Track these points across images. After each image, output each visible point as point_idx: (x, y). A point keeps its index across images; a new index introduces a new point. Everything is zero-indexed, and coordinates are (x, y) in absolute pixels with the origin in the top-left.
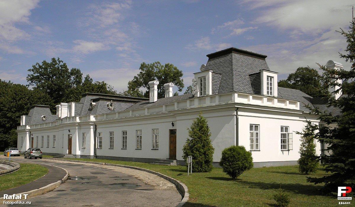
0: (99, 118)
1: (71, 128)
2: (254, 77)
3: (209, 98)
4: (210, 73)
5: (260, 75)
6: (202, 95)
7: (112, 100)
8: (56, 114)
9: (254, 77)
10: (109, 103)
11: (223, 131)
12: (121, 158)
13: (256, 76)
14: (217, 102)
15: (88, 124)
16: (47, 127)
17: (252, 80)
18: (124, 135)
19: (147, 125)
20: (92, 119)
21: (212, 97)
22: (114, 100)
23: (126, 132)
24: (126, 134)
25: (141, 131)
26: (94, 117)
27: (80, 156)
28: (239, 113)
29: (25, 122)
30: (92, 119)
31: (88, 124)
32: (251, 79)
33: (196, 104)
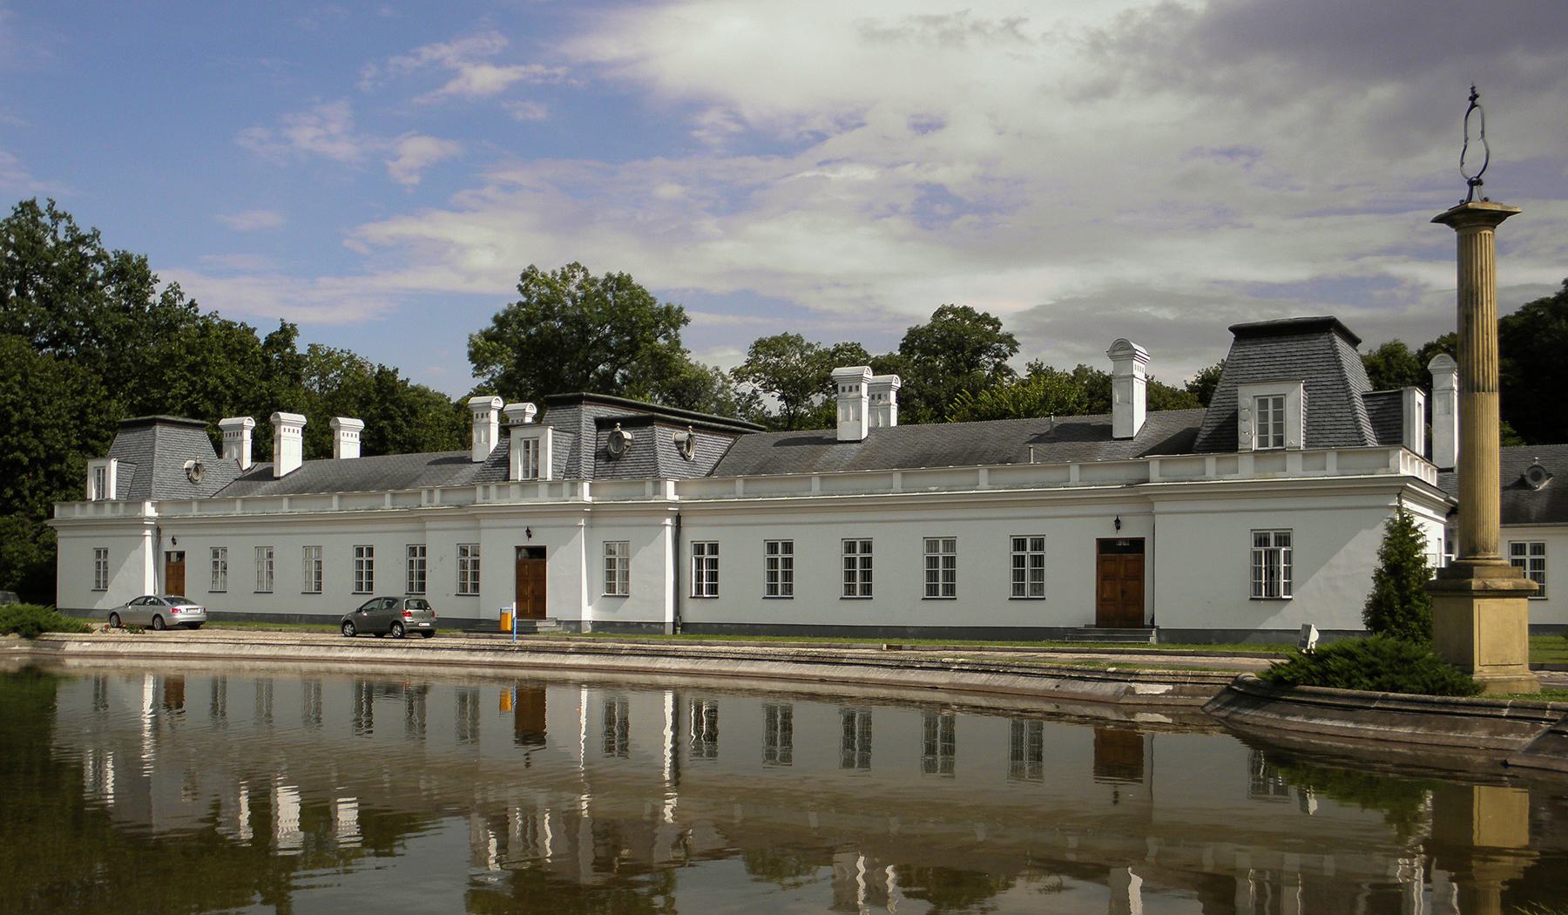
0: (692, 490)
1: (539, 522)
2: (1381, 403)
3: (546, 486)
4: (550, 431)
5: (1401, 399)
6: (528, 477)
7: (690, 424)
8: (331, 456)
9: (1381, 403)
10: (682, 435)
11: (1350, 546)
12: (700, 626)
13: (1387, 402)
14: (121, 511)
15: (139, 523)
16: (296, 511)
17: (1372, 410)
18: (100, 557)
19: (358, 535)
20: (149, 510)
21: (115, 504)
22: (697, 427)
23: (106, 552)
24: (105, 557)
25: (319, 548)
26: (153, 505)
27: (590, 627)
28: (1158, 507)
29: (117, 478)
30: (149, 510)
31: (139, 523)
32: (1370, 408)
33: (514, 498)
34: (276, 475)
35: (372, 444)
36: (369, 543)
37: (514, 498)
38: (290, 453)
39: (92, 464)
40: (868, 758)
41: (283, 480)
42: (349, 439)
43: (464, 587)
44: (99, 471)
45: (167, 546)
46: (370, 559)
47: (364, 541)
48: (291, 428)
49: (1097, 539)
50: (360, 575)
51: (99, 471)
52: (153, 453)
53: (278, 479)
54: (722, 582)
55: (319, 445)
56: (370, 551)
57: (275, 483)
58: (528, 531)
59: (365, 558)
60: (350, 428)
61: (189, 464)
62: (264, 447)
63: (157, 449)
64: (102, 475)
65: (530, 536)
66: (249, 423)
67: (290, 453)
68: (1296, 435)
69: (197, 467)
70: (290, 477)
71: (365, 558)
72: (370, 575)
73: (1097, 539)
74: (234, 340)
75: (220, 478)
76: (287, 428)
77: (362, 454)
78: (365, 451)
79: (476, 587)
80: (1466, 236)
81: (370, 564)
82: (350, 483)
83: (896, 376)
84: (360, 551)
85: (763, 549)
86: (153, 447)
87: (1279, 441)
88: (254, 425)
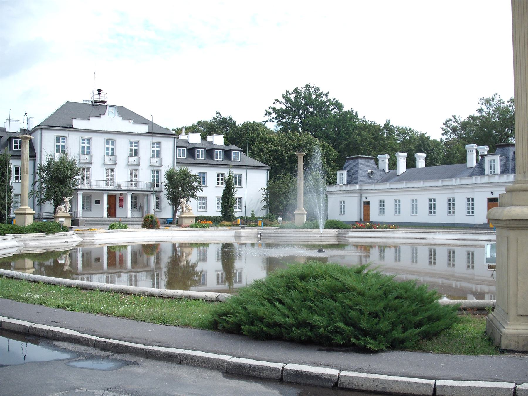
23: (344, 202)
34: (398, 174)
35: (429, 163)
36: (416, 198)
37: (485, 179)
38: (402, 166)
39: (339, 173)
40: (474, 262)
41: (400, 176)
42: (421, 160)
43: (468, 212)
44: (341, 175)
45: (364, 200)
46: (473, 202)
47: (432, 197)
48: (403, 158)
49: (100, 204)
50: (431, 209)
51: (341, 175)
52: (358, 168)
53: (398, 176)
54: (436, 211)
55: (411, 163)
56: (434, 200)
57: (398, 178)
58: (492, 192)
59: (432, 203)
60: (422, 157)
61: (369, 171)
62: (393, 165)
63: (359, 167)
64: (342, 175)
65: (492, 194)
66: (387, 156)
67: (402, 166)
68: (345, 181)
69: (372, 173)
70: (403, 175)
71: (432, 203)
72: (434, 209)
73: (100, 204)
74: (373, 129)
75: (379, 176)
76: (401, 158)
77: (426, 166)
78: (427, 165)
79: (473, 212)
80: (157, 185)
81: (434, 205)
82: (421, 176)
83: (486, 146)
84: (431, 200)
85: (465, 200)
86: (358, 166)
87: (494, 172)
88: (389, 157)
